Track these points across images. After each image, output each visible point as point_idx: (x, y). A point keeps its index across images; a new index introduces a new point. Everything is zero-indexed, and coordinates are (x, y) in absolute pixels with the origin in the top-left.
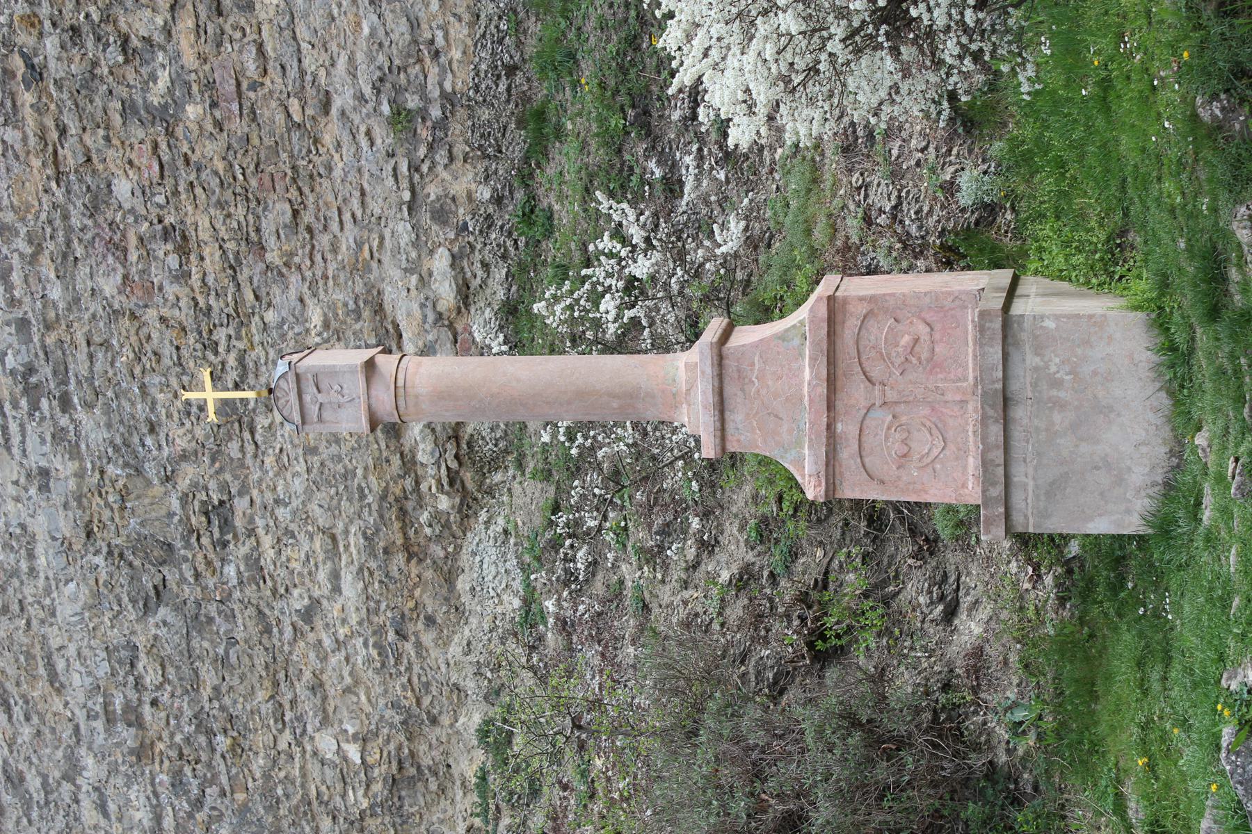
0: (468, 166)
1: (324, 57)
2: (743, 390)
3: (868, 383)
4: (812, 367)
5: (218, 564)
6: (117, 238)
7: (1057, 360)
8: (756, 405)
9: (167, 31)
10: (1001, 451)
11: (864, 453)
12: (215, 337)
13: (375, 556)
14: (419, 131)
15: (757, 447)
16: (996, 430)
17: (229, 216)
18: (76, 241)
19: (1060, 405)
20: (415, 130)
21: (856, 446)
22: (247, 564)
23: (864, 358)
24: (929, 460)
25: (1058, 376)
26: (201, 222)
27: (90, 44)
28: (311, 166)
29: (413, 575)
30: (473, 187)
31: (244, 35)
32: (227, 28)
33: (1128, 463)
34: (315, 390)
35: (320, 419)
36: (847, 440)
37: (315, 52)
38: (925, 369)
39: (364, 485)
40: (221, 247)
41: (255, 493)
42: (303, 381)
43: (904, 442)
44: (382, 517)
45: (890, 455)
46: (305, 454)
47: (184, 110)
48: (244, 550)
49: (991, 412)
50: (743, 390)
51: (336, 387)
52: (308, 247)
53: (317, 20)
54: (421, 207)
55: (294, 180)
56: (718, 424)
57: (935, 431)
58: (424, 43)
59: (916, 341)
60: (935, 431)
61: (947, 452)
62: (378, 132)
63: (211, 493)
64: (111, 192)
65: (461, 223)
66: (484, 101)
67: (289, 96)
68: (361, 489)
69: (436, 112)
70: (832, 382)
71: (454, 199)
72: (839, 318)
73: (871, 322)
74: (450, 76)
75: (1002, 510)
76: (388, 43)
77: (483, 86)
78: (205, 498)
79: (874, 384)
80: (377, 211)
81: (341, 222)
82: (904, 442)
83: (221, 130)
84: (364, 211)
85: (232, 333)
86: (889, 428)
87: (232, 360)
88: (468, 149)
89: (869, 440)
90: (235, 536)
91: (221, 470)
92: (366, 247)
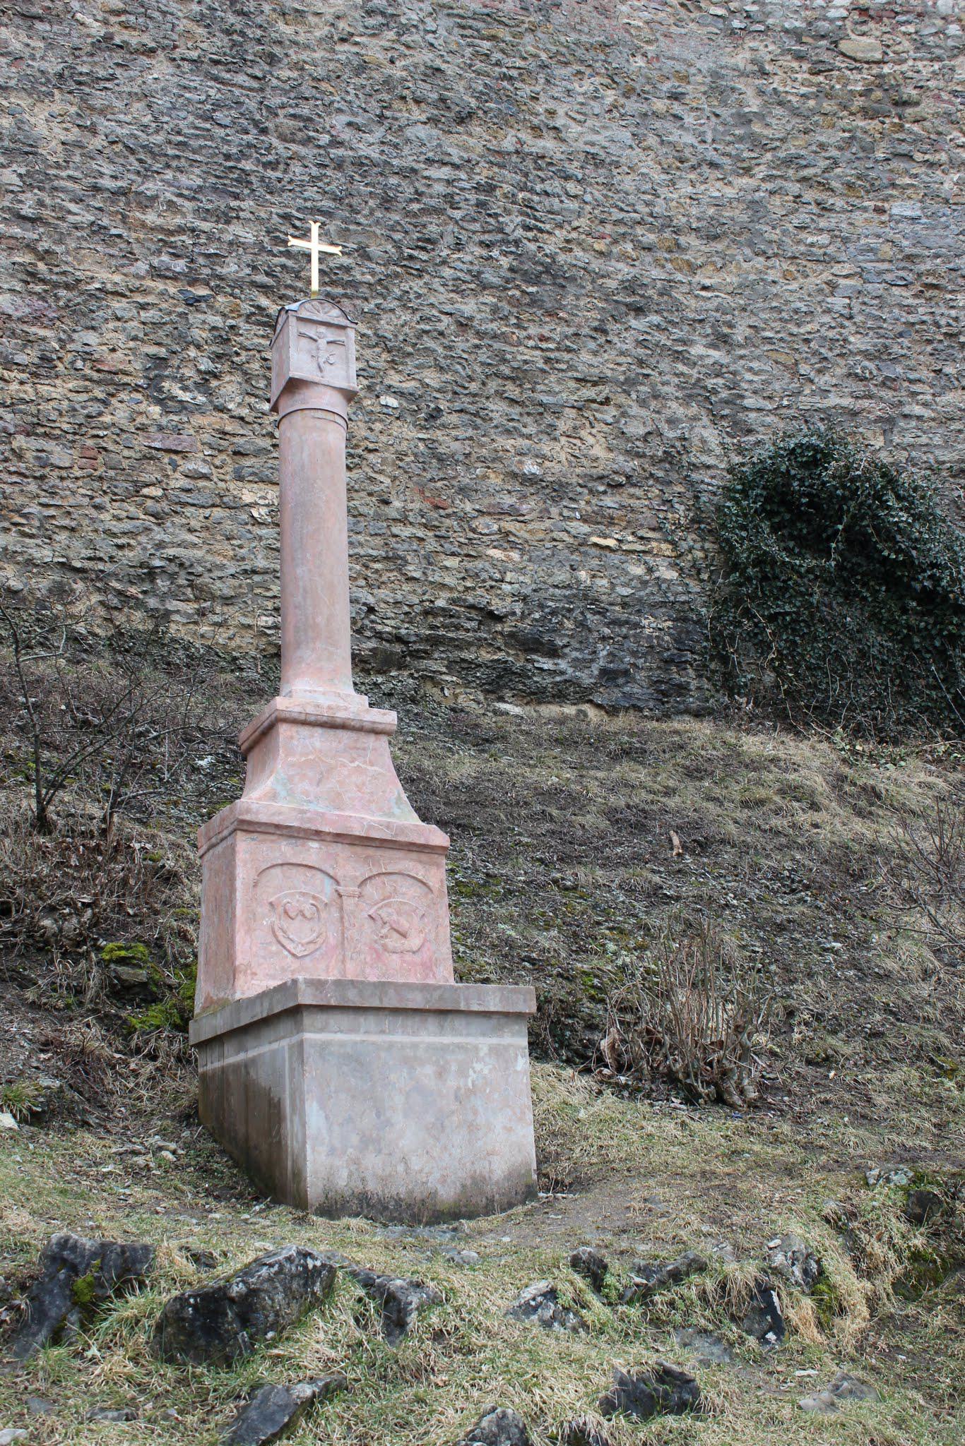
3: (361, 879)
6: (45, 320)
7: (486, 1071)
9: (222, 409)
11: (285, 868)
17: (61, 415)
18: (46, 288)
19: (441, 1074)
23: (385, 879)
25: (471, 1072)
26: (58, 390)
27: (214, 348)
32: (224, 456)
35: (301, 335)
37: (201, 518)
38: (376, 942)
45: (286, 896)
49: (436, 994)
52: (28, 473)
53: (228, 526)
56: (312, 718)
57: (312, 947)
59: (404, 935)
64: (88, 328)
69: (152, 602)
72: (424, 857)
75: (333, 1003)
79: (359, 886)
83: (138, 429)
86: (314, 897)
89: (298, 876)
92: (24, 521)
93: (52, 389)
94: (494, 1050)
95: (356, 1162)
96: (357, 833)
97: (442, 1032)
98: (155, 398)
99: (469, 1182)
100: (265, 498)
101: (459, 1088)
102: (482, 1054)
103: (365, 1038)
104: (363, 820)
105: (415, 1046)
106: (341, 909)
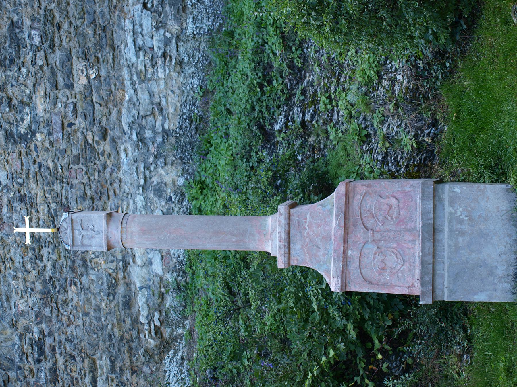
0: (174, 168)
1: (106, 111)
2: (300, 233)
3: (365, 229)
4: (336, 220)
5: (35, 371)
7: (461, 209)
8: (307, 241)
10: (431, 257)
12: (42, 253)
13: (115, 371)
14: (150, 149)
15: (307, 263)
16: (429, 245)
19: (462, 233)
20: (148, 148)
21: (358, 263)
22: (50, 372)
24: (395, 271)
25: (461, 217)
28: (95, 166)
29: (134, 382)
30: (176, 178)
31: (68, 99)
32: (60, 96)
33: (496, 264)
34: (80, 228)
36: (353, 259)
37: (101, 108)
39: (111, 333)
40: (48, 206)
41: (56, 335)
42: (74, 223)
43: (382, 261)
44: (119, 350)
45: (375, 268)
46: (82, 316)
47: (35, 136)
48: (49, 365)
49: (426, 236)
50: (300, 233)
51: (91, 227)
53: (104, 93)
54: (149, 188)
55: (86, 173)
56: (287, 250)
57: (399, 256)
58: (156, 104)
60: (399, 256)
61: (405, 267)
62: (130, 149)
63: (34, 334)
65: (168, 197)
66: (184, 134)
67: (87, 131)
68: (110, 336)
69: (159, 139)
70: (346, 227)
71: (165, 184)
72: (351, 195)
73: (368, 197)
74: (167, 121)
75: (431, 288)
76: (138, 104)
77: (184, 126)
78: (31, 337)
79: (368, 230)
80: (127, 190)
81: (108, 196)
82: (382, 261)
83: (53, 147)
84: (120, 190)
85: (50, 251)
86: (375, 254)
87: (49, 265)
88: (174, 159)
89: (365, 260)
90: (45, 358)
91: (40, 323)
93: (39, 196)
94: (452, 203)
95: (500, 279)
96: (343, 232)
97: (443, 231)
98: (31, 137)
99: (511, 223)
100: (82, 71)
101: (469, 224)
102: (453, 211)
103: (446, 271)
104: (334, 225)
105: (450, 246)
106: (380, 240)
